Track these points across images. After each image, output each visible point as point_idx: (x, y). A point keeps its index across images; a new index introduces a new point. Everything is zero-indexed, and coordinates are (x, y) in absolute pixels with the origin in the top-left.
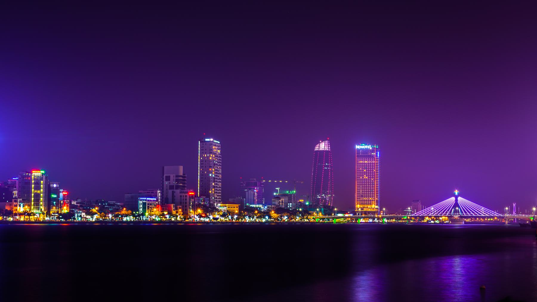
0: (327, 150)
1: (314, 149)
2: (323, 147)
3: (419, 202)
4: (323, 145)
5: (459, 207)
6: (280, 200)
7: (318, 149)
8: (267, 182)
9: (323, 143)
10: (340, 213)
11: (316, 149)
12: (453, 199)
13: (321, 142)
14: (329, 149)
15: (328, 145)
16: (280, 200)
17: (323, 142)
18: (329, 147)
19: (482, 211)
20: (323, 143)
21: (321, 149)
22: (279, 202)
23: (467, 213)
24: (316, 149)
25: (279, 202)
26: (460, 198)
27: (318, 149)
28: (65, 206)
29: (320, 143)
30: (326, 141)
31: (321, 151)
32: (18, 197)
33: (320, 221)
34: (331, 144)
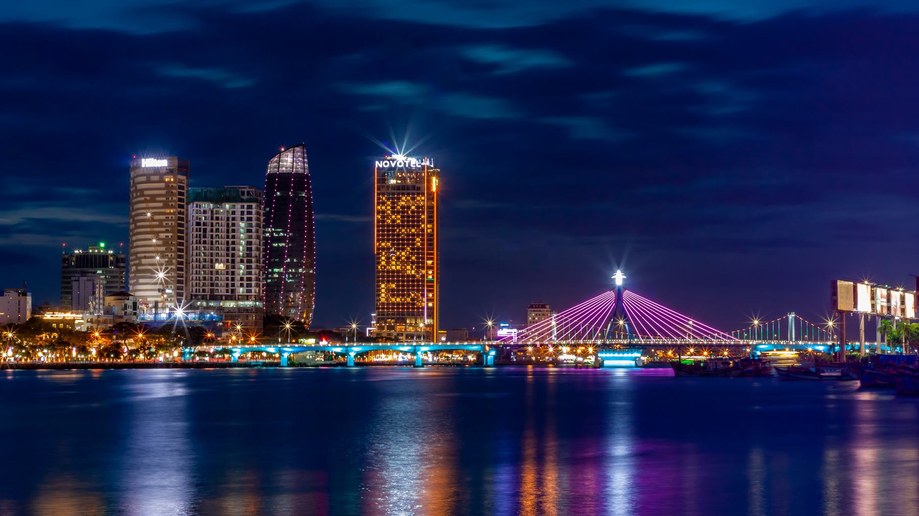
0: (301, 171)
1: (266, 168)
2: (289, 164)
3: (545, 309)
4: (290, 159)
5: (625, 317)
6: (128, 299)
7: (276, 170)
8: (313, 286)
9: (290, 155)
10: (311, 338)
11: (271, 168)
12: (610, 295)
13: (283, 149)
14: (304, 169)
15: (304, 158)
16: (127, 302)
17: (290, 152)
18: (306, 165)
19: (689, 330)
20: (290, 155)
21: (284, 169)
22: (126, 305)
23: (674, 339)
24: (271, 168)
25: (126, 305)
26: (627, 294)
27: (276, 170)
28: (10, 338)
29: (280, 152)
30: (297, 149)
31: (283, 173)
32: (280, 343)
33: (21, 359)
34: (312, 159)
